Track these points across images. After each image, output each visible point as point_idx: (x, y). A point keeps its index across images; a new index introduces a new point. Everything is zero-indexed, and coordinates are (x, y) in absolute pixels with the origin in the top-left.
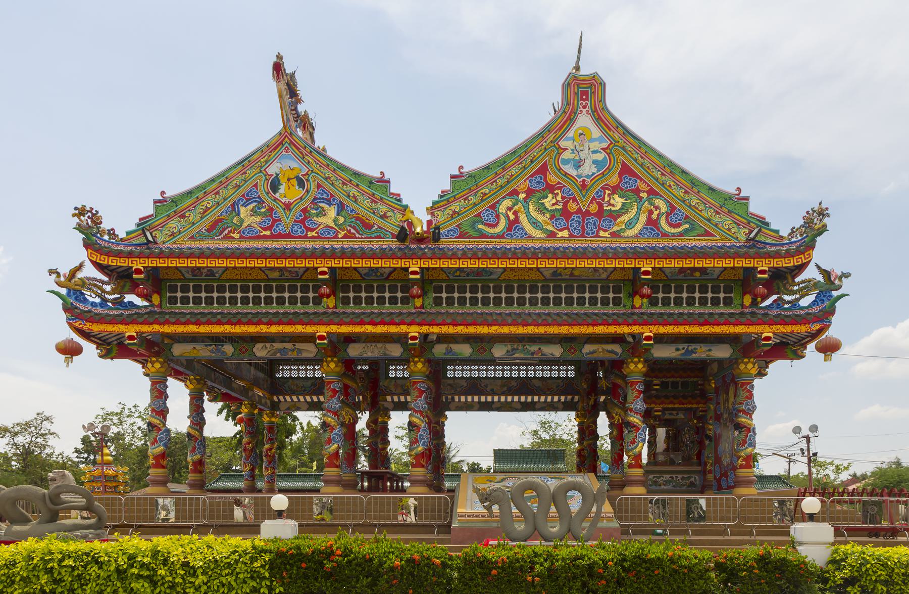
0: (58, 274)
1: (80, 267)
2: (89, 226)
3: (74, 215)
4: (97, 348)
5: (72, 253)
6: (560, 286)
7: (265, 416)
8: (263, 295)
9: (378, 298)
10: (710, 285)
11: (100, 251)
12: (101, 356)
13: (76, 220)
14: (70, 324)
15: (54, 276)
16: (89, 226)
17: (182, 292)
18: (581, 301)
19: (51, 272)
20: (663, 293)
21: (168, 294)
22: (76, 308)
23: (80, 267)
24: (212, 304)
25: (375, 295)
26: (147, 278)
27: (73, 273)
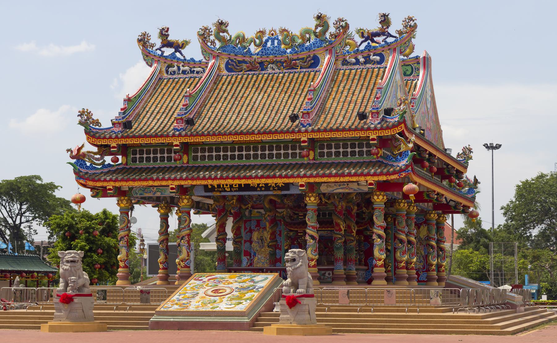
0: (72, 152)
1: (83, 146)
2: (87, 121)
3: (78, 116)
4: (91, 191)
5: (79, 139)
6: (150, 150)
7: (83, 243)
8: (207, 154)
9: (208, 156)
10: (267, 146)
11: (93, 136)
12: (92, 196)
13: (79, 118)
14: (77, 180)
15: (69, 153)
16: (87, 121)
17: (239, 151)
18: (263, 156)
19: (68, 151)
20: (276, 150)
21: (193, 154)
22: (81, 172)
23: (83, 146)
24: (280, 157)
25: (290, 152)
26: (181, 148)
27: (79, 149)
